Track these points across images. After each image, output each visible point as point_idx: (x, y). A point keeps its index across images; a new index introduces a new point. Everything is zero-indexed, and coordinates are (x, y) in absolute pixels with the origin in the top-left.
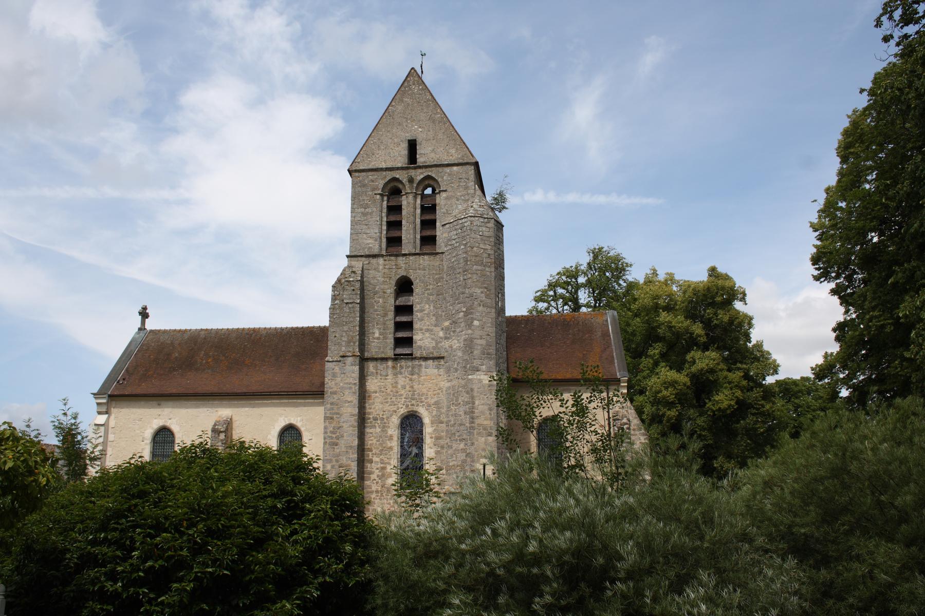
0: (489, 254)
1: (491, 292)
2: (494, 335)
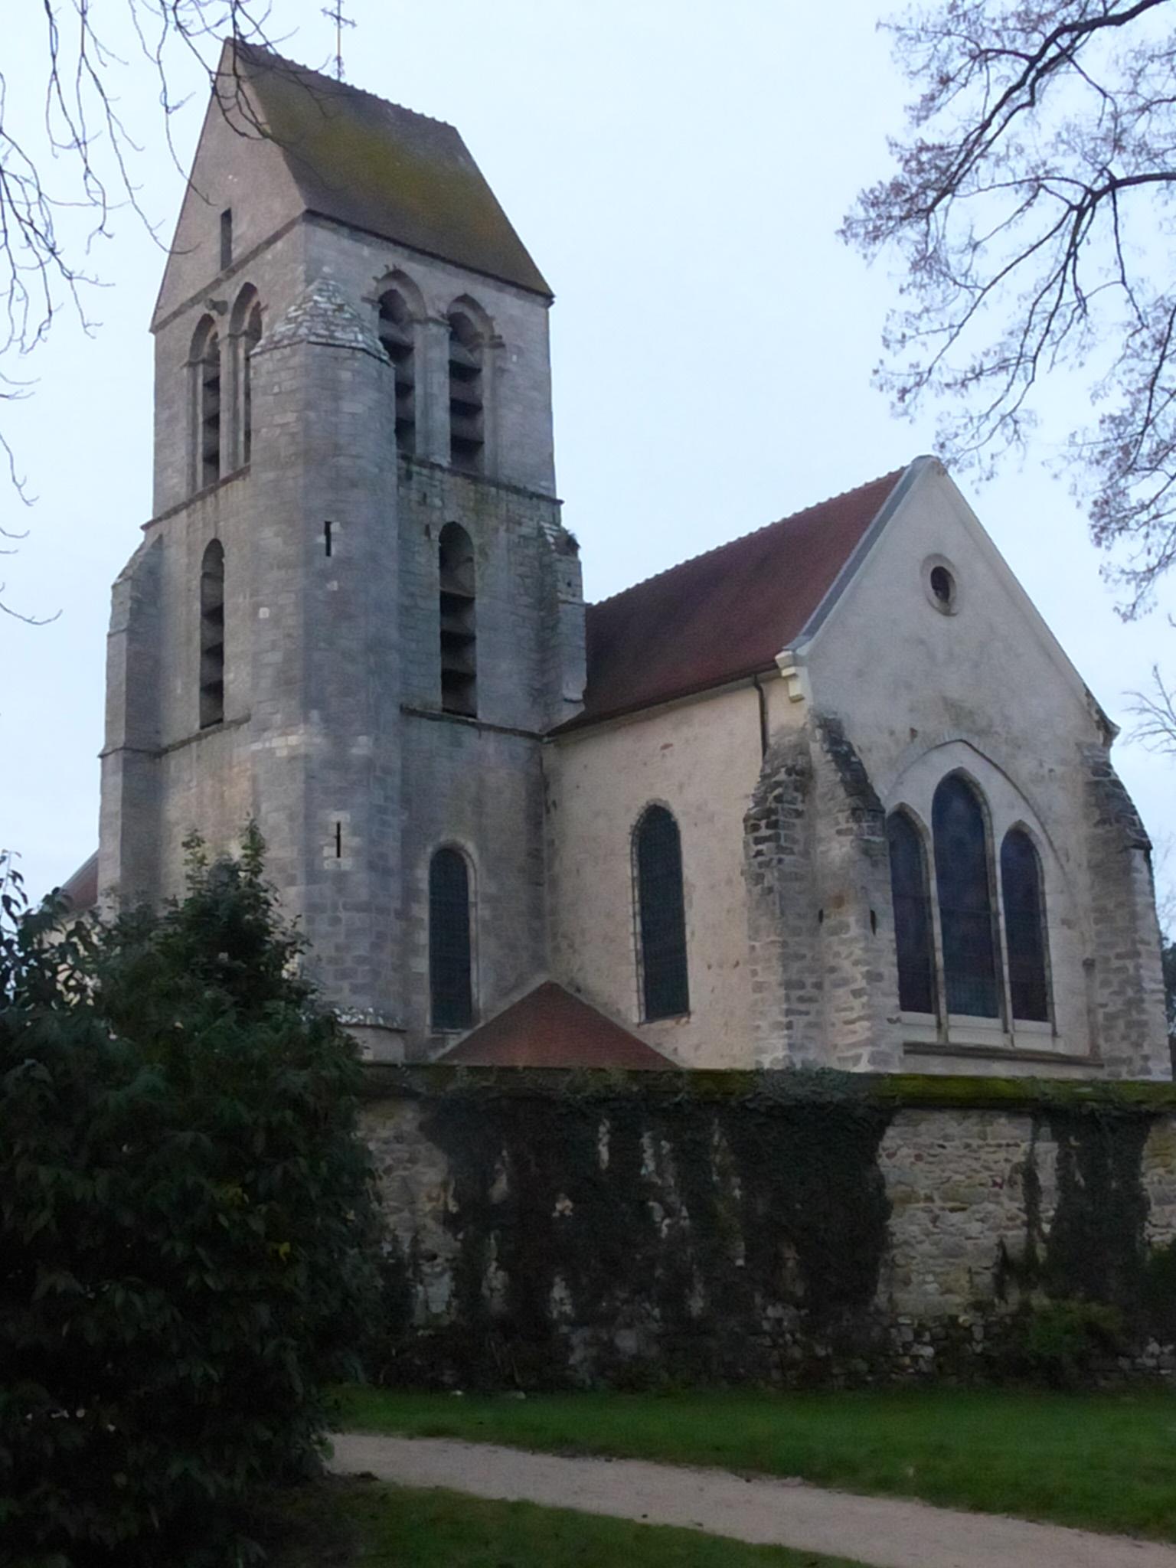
0: (293, 435)
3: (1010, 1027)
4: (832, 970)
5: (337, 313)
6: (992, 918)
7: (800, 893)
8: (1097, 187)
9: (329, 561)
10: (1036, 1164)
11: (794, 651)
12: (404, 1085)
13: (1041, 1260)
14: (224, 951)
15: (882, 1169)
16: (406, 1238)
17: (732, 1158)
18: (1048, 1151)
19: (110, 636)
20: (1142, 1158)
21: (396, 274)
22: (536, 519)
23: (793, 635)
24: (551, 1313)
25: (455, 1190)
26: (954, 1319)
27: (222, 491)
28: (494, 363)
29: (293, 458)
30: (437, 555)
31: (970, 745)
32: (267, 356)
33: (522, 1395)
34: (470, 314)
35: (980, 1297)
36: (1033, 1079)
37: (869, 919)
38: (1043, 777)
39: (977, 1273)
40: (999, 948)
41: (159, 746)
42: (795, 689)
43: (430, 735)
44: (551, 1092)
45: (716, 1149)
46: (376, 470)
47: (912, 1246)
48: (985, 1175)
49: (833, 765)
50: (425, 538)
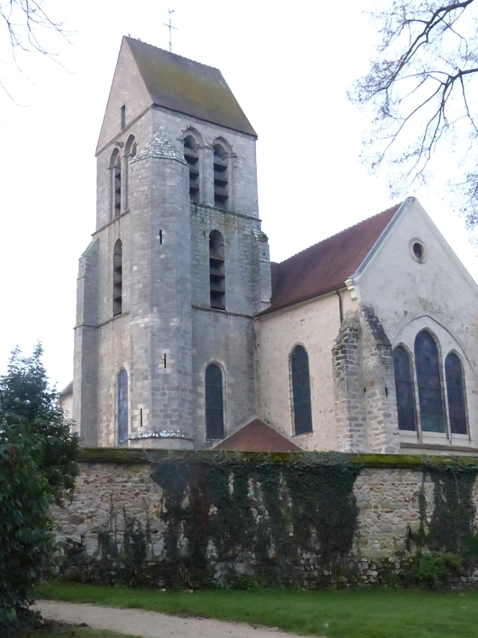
0: (147, 195)
3: (450, 437)
4: (370, 413)
5: (165, 145)
6: (442, 390)
7: (356, 380)
8: (454, 75)
9: (161, 246)
10: (424, 492)
11: (352, 279)
12: (144, 458)
13: (426, 534)
14: (17, 397)
15: (355, 494)
16: (144, 523)
17: (288, 489)
18: (430, 487)
19: (78, 279)
20: (472, 490)
21: (191, 129)
22: (250, 228)
23: (353, 273)
24: (207, 556)
25: (166, 503)
26: (387, 559)
27: (121, 219)
28: (232, 164)
29: (147, 204)
30: (208, 243)
31: (431, 318)
32: (136, 163)
33: (191, 591)
34: (194, 136)
35: (398, 550)
36: (424, 456)
37: (384, 391)
38: (464, 331)
39: (398, 539)
40: (445, 403)
41: (97, 324)
42: (353, 295)
43: (206, 317)
44: (208, 462)
45: (281, 486)
46: (181, 209)
47: (368, 528)
48: (401, 497)
49: (369, 327)
50: (203, 236)
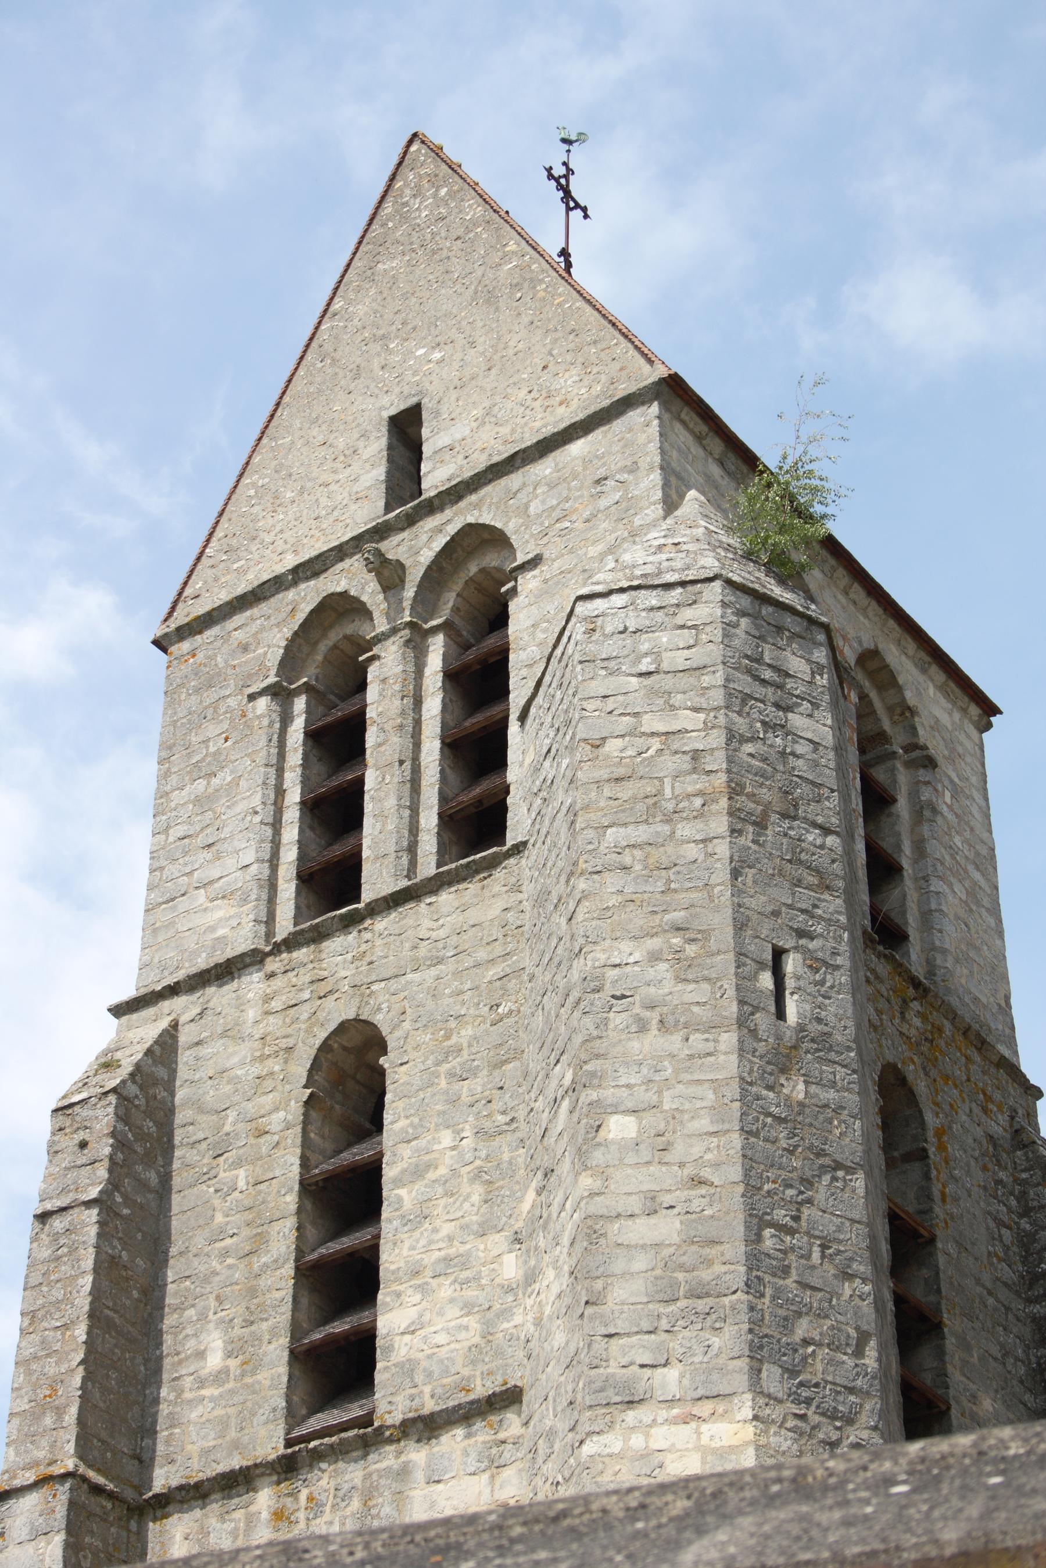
0: (696, 755)
1: (713, 946)
2: (735, 1172)
